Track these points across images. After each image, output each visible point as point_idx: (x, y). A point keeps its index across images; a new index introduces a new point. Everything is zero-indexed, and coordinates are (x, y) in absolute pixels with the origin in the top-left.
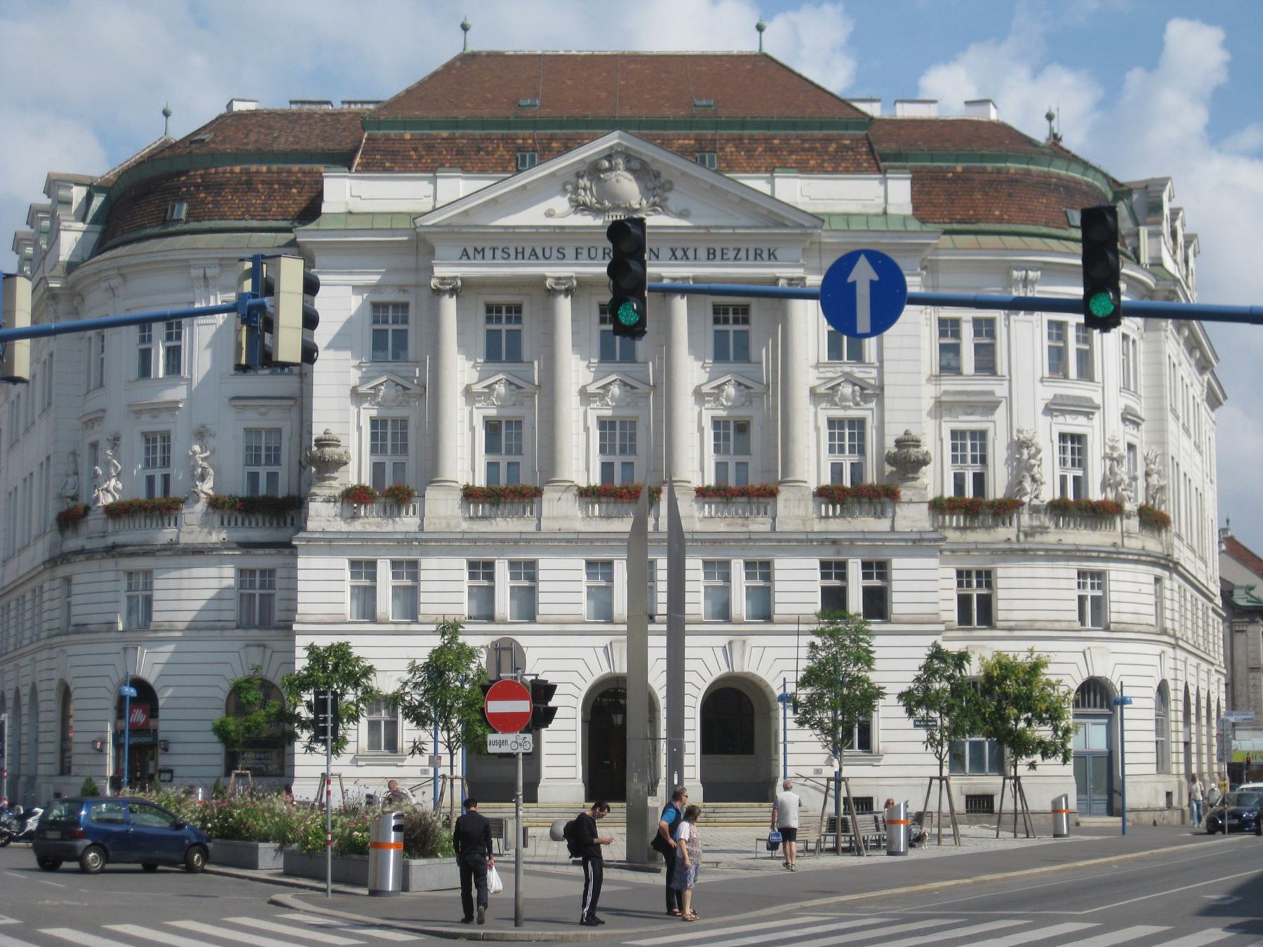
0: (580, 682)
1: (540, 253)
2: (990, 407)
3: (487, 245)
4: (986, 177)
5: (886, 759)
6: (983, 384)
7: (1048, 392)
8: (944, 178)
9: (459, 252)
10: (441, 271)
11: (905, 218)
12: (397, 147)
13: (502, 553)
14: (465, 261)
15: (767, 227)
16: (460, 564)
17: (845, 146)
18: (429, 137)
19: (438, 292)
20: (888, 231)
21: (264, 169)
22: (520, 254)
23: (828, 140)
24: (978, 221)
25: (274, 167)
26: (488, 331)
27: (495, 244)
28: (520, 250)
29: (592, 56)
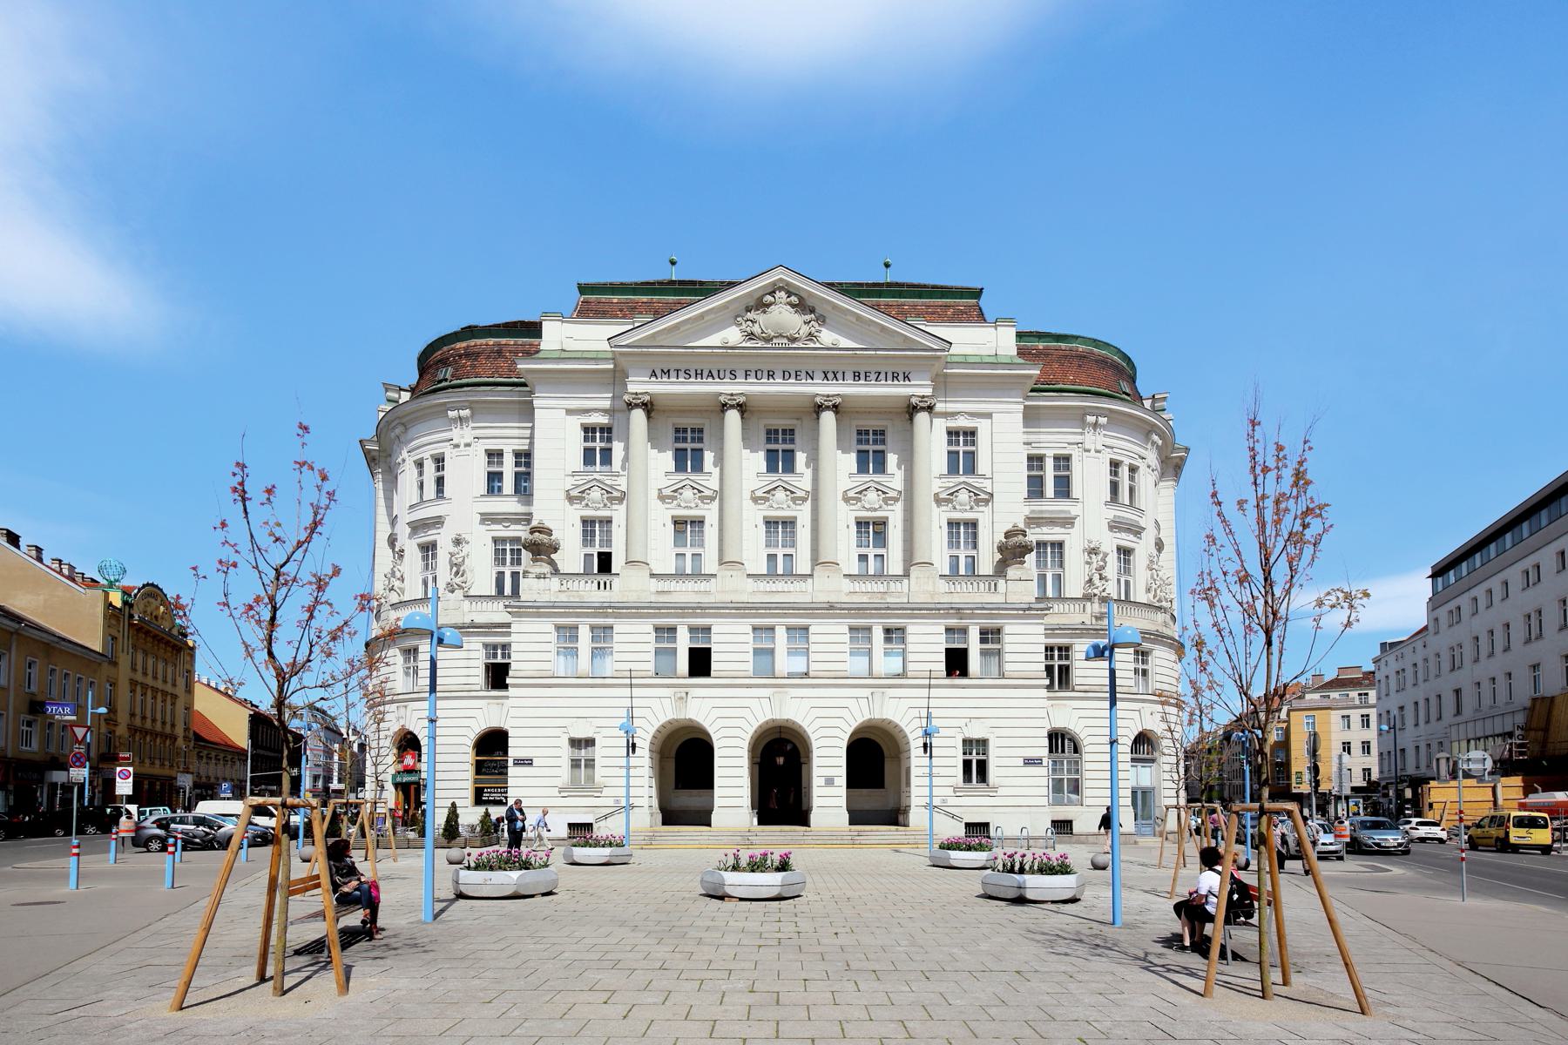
0: (743, 735)
1: (715, 373)
2: (438, 522)
5: (1001, 791)
6: (1062, 506)
7: (1112, 513)
10: (632, 388)
12: (607, 308)
16: (646, 627)
18: (632, 301)
19: (631, 406)
22: (699, 374)
29: (760, 764)
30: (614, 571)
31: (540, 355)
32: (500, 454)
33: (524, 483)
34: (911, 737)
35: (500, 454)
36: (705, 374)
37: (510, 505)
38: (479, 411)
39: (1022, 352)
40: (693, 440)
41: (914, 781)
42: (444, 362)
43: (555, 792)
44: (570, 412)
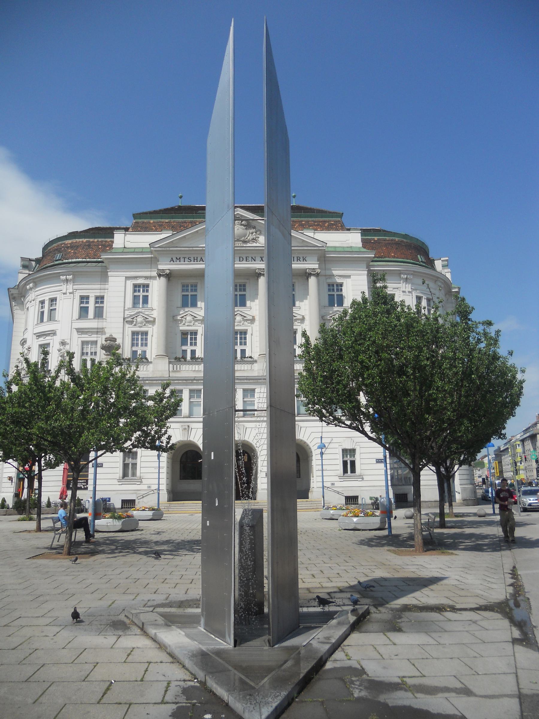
3: (182, 256)
4: (387, 242)
8: (370, 242)
9: (170, 259)
11: (359, 248)
13: (186, 384)
14: (172, 262)
15: (235, 604)
17: (332, 224)
18: (160, 222)
20: (353, 252)
21: (96, 240)
23: (325, 222)
24: (385, 257)
25: (100, 240)
26: (183, 295)
27: (184, 256)
28: (196, 258)
30: (104, 317)
31: (113, 251)
32: (88, 297)
33: (99, 313)
34: (313, 449)
35: (88, 297)
36: (199, 259)
37: (90, 323)
38: (77, 277)
39: (365, 243)
40: (192, 290)
41: (314, 458)
42: (58, 250)
43: (116, 482)
44: (127, 278)
